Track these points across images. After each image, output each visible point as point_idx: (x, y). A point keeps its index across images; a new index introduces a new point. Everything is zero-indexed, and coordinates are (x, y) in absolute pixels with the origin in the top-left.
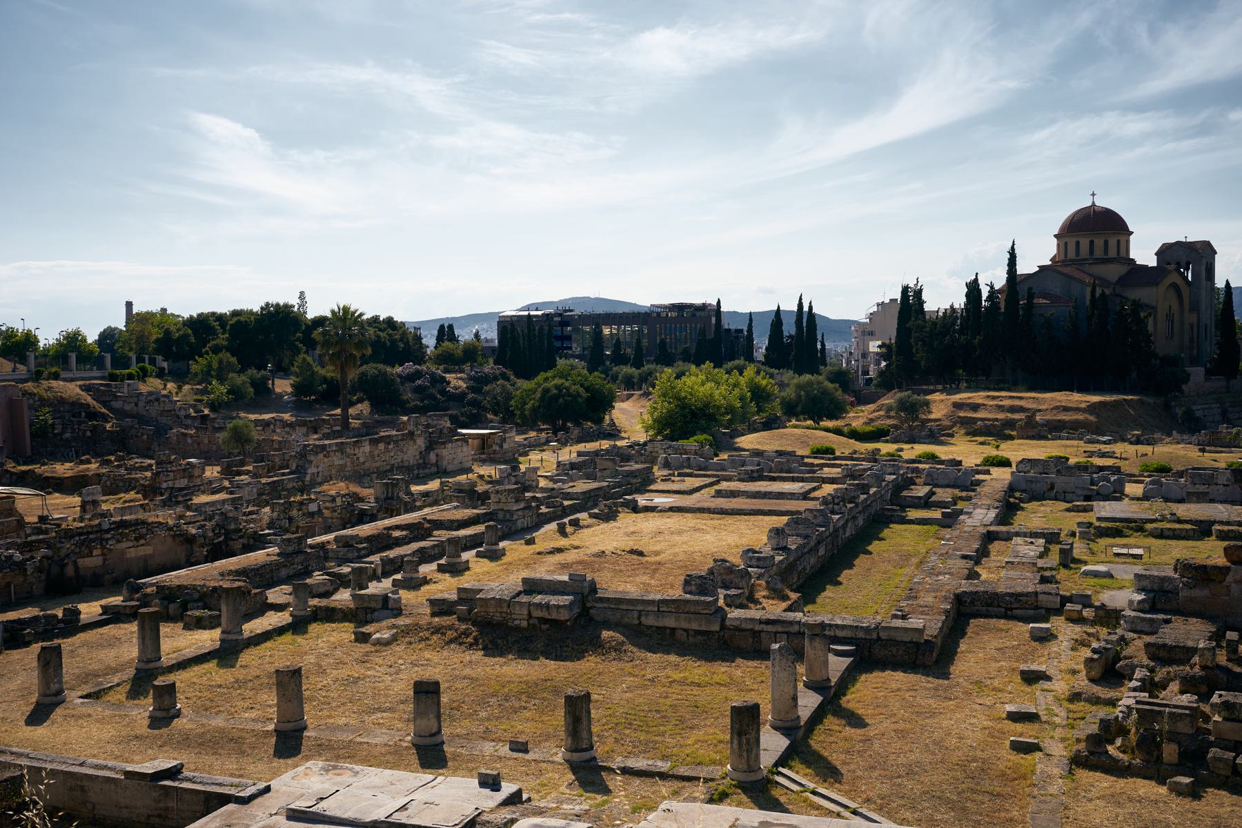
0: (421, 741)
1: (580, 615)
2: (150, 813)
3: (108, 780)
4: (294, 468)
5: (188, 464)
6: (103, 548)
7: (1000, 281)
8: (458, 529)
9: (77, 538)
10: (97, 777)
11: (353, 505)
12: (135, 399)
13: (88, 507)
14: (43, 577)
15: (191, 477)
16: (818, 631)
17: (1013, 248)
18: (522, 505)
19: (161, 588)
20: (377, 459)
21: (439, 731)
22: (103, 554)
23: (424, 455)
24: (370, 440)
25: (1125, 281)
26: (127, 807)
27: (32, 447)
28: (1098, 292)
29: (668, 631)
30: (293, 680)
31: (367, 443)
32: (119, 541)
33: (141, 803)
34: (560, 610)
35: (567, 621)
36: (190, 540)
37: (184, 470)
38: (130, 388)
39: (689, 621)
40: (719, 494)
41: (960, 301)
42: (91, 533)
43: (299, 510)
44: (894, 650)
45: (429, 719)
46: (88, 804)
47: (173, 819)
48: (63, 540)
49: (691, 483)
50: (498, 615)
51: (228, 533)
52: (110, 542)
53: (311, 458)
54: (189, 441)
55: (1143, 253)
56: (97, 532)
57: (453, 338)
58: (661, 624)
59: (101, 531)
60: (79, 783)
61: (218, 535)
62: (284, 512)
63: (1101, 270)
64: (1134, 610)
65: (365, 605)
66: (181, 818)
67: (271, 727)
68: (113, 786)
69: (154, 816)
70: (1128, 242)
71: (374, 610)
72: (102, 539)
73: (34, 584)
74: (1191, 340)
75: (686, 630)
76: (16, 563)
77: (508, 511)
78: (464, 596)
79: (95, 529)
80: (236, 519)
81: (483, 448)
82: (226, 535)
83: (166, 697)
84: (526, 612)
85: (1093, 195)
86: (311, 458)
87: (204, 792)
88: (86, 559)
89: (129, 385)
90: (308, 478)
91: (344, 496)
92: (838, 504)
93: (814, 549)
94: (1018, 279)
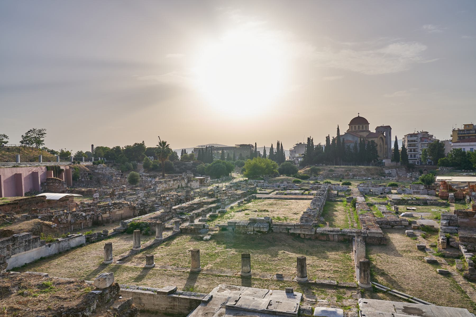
0: (243, 274)
1: (269, 229)
2: (167, 307)
3: (150, 295)
4: (153, 188)
5: (123, 187)
6: (110, 211)
7: (335, 136)
8: (210, 204)
9: (102, 208)
10: (146, 294)
11: (178, 198)
12: (102, 170)
13: (95, 200)
14: (91, 221)
15: (124, 191)
16: (360, 234)
17: (338, 128)
19: (444, 182)
21: (250, 271)
22: (109, 213)
23: (187, 184)
24: (173, 180)
25: (368, 137)
26: (157, 305)
27: (73, 183)
28: (362, 139)
29: (298, 234)
30: (197, 254)
32: (114, 209)
33: (163, 304)
34: (264, 228)
35: (266, 232)
36: (134, 208)
37: (122, 189)
38: (100, 166)
39: (305, 231)
40: (277, 194)
41: (324, 143)
42: (106, 207)
43: (164, 199)
44: (374, 240)
45: (247, 267)
46: (142, 304)
47: (176, 309)
48: (98, 209)
49: (268, 191)
50: (243, 230)
51: (144, 206)
52: (112, 209)
53: (157, 185)
54: (118, 181)
55: (372, 129)
56: (108, 206)
58: (295, 232)
59: (109, 206)
60: (138, 296)
61: (142, 207)
62: (160, 200)
63: (362, 134)
64: (444, 226)
65: (197, 228)
66: (180, 309)
67: (189, 270)
68: (152, 297)
69: (168, 308)
70: (368, 126)
71: (200, 229)
72: (109, 208)
73: (88, 223)
74: (386, 152)
75: (304, 234)
76: (83, 216)
77: (224, 199)
78: (230, 224)
79: (107, 205)
80: (146, 202)
81: (201, 182)
82: (144, 207)
83: (151, 260)
84: (253, 229)
85: (359, 114)
86: (157, 185)
87: (190, 299)
88: (104, 215)
89: (100, 165)
90: (157, 191)
91: (176, 195)
92: (321, 196)
93: (321, 209)
94: (340, 136)
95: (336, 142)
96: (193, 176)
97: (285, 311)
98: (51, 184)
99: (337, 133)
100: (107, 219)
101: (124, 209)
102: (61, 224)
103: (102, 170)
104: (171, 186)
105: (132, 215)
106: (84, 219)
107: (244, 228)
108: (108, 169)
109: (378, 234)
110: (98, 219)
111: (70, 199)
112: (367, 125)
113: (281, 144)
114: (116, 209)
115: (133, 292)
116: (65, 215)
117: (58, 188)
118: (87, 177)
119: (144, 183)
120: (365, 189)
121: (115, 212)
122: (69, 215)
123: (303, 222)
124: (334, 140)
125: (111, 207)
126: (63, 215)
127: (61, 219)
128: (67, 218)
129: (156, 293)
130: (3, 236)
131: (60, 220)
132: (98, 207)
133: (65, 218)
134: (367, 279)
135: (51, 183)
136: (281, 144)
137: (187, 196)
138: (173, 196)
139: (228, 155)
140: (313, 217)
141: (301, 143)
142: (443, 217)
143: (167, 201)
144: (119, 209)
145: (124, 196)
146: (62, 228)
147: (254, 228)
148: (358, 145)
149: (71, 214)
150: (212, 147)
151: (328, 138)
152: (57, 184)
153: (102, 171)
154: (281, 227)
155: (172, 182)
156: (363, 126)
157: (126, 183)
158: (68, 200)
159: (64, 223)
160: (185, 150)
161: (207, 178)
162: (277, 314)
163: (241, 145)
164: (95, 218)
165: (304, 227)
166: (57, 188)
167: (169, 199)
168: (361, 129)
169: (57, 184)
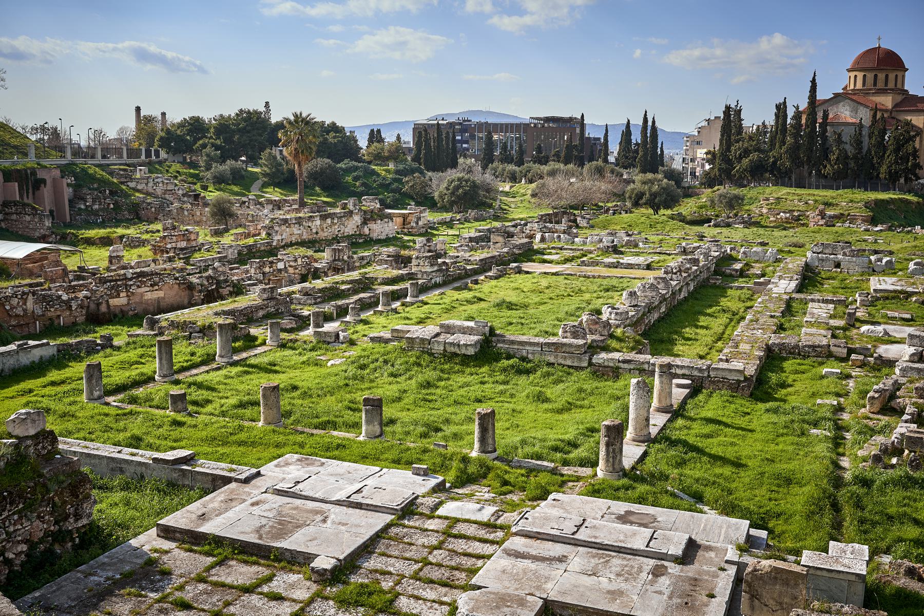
6: (127, 291)
7: (804, 105)
9: (108, 284)
10: (132, 461)
13: (113, 261)
15: (189, 240)
18: (436, 268)
20: (325, 230)
22: (128, 296)
31: (318, 218)
32: (139, 287)
34: (468, 348)
36: (190, 287)
37: (184, 235)
39: (565, 358)
42: (119, 280)
43: (270, 267)
51: (218, 283)
52: (133, 288)
54: (186, 213)
56: (123, 279)
57: (381, 140)
59: (126, 279)
60: (118, 465)
61: (211, 284)
62: (259, 268)
70: (903, 77)
76: (63, 301)
78: (395, 334)
84: (442, 348)
85: (879, 39)
89: (141, 170)
92: (675, 273)
94: (817, 103)
96: (378, 206)
97: (380, 504)
98: (14, 217)
99: (808, 94)
100: (122, 311)
101: (166, 287)
102: (10, 316)
103: (145, 181)
104: (317, 233)
105: (186, 301)
106: (64, 308)
107: (424, 344)
108: (159, 180)
110: (98, 309)
111: (52, 257)
112: (900, 74)
113: (654, 122)
114: (145, 286)
115: (109, 458)
116: (19, 297)
117: (31, 226)
118: (108, 201)
119: (250, 221)
121: (142, 295)
122: (29, 297)
123: (566, 337)
124: (798, 115)
125: (131, 283)
126: (16, 297)
127: (11, 305)
128: (25, 304)
129: (151, 462)
130: (394, 462)
131: (8, 307)
132: (97, 281)
133: (21, 304)
134: (613, 462)
135: (13, 214)
136: (654, 122)
137: (335, 260)
138: (296, 261)
139: (504, 147)
140: (604, 327)
141: (776, 115)
142: (911, 339)
143: (280, 271)
144: (151, 288)
145: (185, 254)
146: (13, 326)
148: (865, 132)
149: (33, 296)
150: (464, 121)
151: (781, 109)
152: (27, 216)
153: (147, 184)
154: (511, 347)
155: (318, 222)
156: (887, 76)
157: (204, 219)
158: (47, 259)
159: (17, 316)
160: (379, 131)
161: (421, 212)
162: (363, 507)
163: (548, 120)
164: (92, 306)
166: (27, 227)
167: (285, 267)
168: (881, 85)
169: (28, 218)
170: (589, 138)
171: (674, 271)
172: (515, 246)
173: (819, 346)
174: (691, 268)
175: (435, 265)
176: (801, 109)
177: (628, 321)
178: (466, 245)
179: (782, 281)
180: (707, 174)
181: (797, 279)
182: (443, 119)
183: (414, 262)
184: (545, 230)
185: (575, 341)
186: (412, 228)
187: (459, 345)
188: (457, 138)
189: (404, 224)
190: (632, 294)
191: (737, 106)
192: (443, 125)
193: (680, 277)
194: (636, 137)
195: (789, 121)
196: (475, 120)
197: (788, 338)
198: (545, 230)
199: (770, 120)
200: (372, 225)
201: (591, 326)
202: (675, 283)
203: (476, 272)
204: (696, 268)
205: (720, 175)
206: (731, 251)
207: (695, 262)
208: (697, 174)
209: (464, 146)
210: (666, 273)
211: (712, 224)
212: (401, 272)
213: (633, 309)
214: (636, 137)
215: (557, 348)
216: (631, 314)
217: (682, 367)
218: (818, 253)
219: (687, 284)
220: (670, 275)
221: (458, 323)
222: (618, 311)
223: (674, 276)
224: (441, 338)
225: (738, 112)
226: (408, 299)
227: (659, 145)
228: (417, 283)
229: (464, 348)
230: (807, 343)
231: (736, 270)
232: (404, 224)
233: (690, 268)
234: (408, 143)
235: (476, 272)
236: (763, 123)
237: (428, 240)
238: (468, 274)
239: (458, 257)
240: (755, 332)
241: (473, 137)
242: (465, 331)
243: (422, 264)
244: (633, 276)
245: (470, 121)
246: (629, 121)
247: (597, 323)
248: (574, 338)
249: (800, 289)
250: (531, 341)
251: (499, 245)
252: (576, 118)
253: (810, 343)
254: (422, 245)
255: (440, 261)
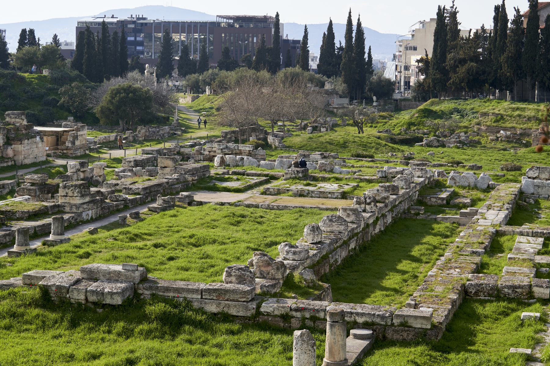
18: (87, 199)
34: (114, 296)
92: (369, 204)
94: (539, 6)
95: (525, 21)
96: (25, 123)
109: (419, 321)
120: (539, 187)
123: (231, 282)
147: (88, 294)
150: (139, 19)
160: (32, 32)
161: (78, 130)
163: (237, 19)
165: (227, 297)
170: (287, 41)
171: (368, 201)
172: (188, 172)
173: (520, 287)
174: (388, 197)
175: (87, 195)
176: (522, 13)
177: (308, 261)
178: (130, 170)
179: (491, 211)
180: (420, 85)
181: (507, 209)
182: (113, 17)
183: (61, 192)
184: (226, 151)
185: (241, 287)
186: (67, 149)
187: (103, 294)
188: (129, 39)
189: (57, 144)
190: (315, 229)
191: (452, 7)
192: (112, 23)
193: (374, 208)
194: (340, 40)
195: (509, 25)
196: (151, 17)
197: (485, 280)
198: (226, 151)
199: (490, 25)
200: (18, 147)
201: (263, 269)
202: (368, 215)
203: (136, 203)
204: (394, 197)
205: (434, 87)
206: (438, 176)
207: (394, 190)
208: (411, 84)
209: (139, 48)
210: (359, 203)
211: (424, 143)
212: (45, 204)
213: (315, 246)
214: (340, 40)
215: (219, 295)
216: (312, 252)
217: (362, 315)
218: (534, 178)
219: (384, 216)
220: (363, 206)
221: (104, 267)
222: (297, 250)
223: (368, 207)
224: (82, 286)
225: (454, 15)
226: (51, 237)
227: (366, 50)
228: (62, 218)
229: (109, 297)
230: (507, 284)
231: (443, 199)
232: (57, 144)
233: (388, 197)
234: (71, 44)
235: (136, 203)
236: (483, 28)
237: (82, 165)
238: (127, 205)
239: (117, 184)
240: (452, 271)
241: (149, 37)
242: (113, 277)
243: (70, 194)
244: (324, 207)
245: (145, 19)
246: (331, 21)
247: (269, 265)
248: (239, 283)
249: (511, 220)
250: (190, 287)
251: (167, 170)
252: (271, 17)
253: (510, 284)
254: (74, 170)
255: (93, 189)
